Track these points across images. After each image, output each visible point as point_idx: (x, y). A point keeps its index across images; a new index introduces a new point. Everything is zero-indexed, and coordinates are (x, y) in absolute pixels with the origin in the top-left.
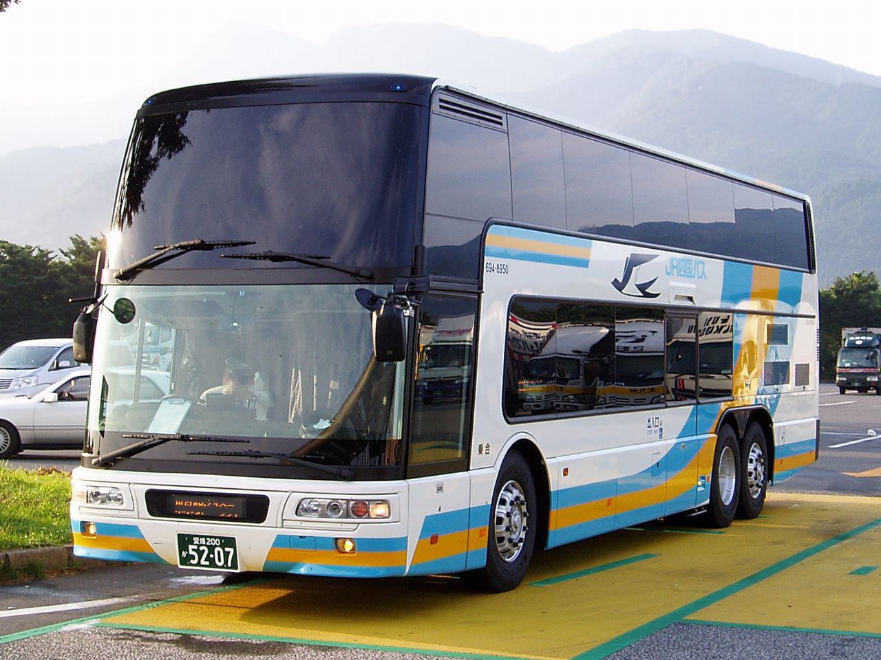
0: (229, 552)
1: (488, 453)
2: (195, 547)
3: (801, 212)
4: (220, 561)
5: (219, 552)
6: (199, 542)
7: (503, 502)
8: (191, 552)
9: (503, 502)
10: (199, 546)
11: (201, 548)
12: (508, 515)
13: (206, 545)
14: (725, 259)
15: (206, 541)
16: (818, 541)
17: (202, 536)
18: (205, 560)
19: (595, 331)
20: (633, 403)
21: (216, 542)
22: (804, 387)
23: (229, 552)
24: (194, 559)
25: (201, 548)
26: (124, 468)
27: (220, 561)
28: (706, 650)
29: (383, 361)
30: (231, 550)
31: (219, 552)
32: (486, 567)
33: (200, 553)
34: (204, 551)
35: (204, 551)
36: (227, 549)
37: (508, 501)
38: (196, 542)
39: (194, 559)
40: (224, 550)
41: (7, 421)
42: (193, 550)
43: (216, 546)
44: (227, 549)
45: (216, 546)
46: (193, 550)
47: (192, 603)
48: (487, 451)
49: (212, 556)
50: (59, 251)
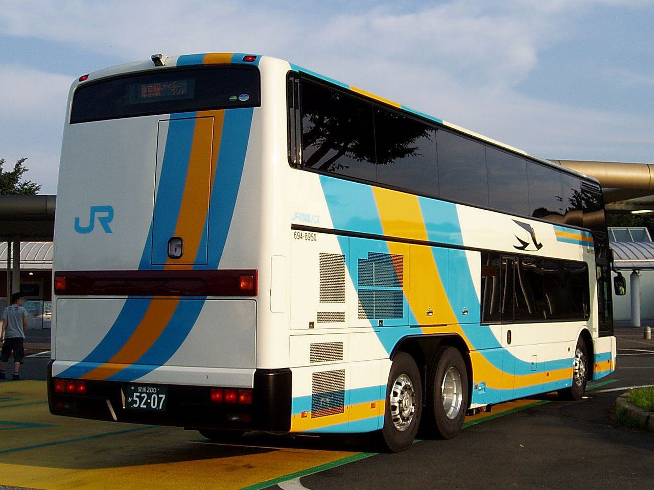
0: (162, 398)
2: (139, 394)
3: (171, 116)
4: (154, 405)
5: (154, 398)
6: (142, 390)
7: (395, 394)
8: (135, 398)
9: (395, 394)
10: (141, 393)
11: (142, 395)
12: (400, 402)
13: (146, 393)
14: (581, 230)
15: (147, 390)
20: (610, 364)
23: (162, 398)
24: (136, 404)
25: (142, 395)
27: (154, 405)
28: (509, 460)
29: (594, 247)
31: (154, 398)
33: (141, 399)
34: (144, 397)
35: (144, 397)
36: (160, 396)
37: (399, 392)
38: (140, 391)
39: (136, 404)
40: (158, 396)
42: (137, 396)
43: (153, 393)
44: (160, 396)
46: (137, 396)
47: (135, 430)
49: (149, 401)
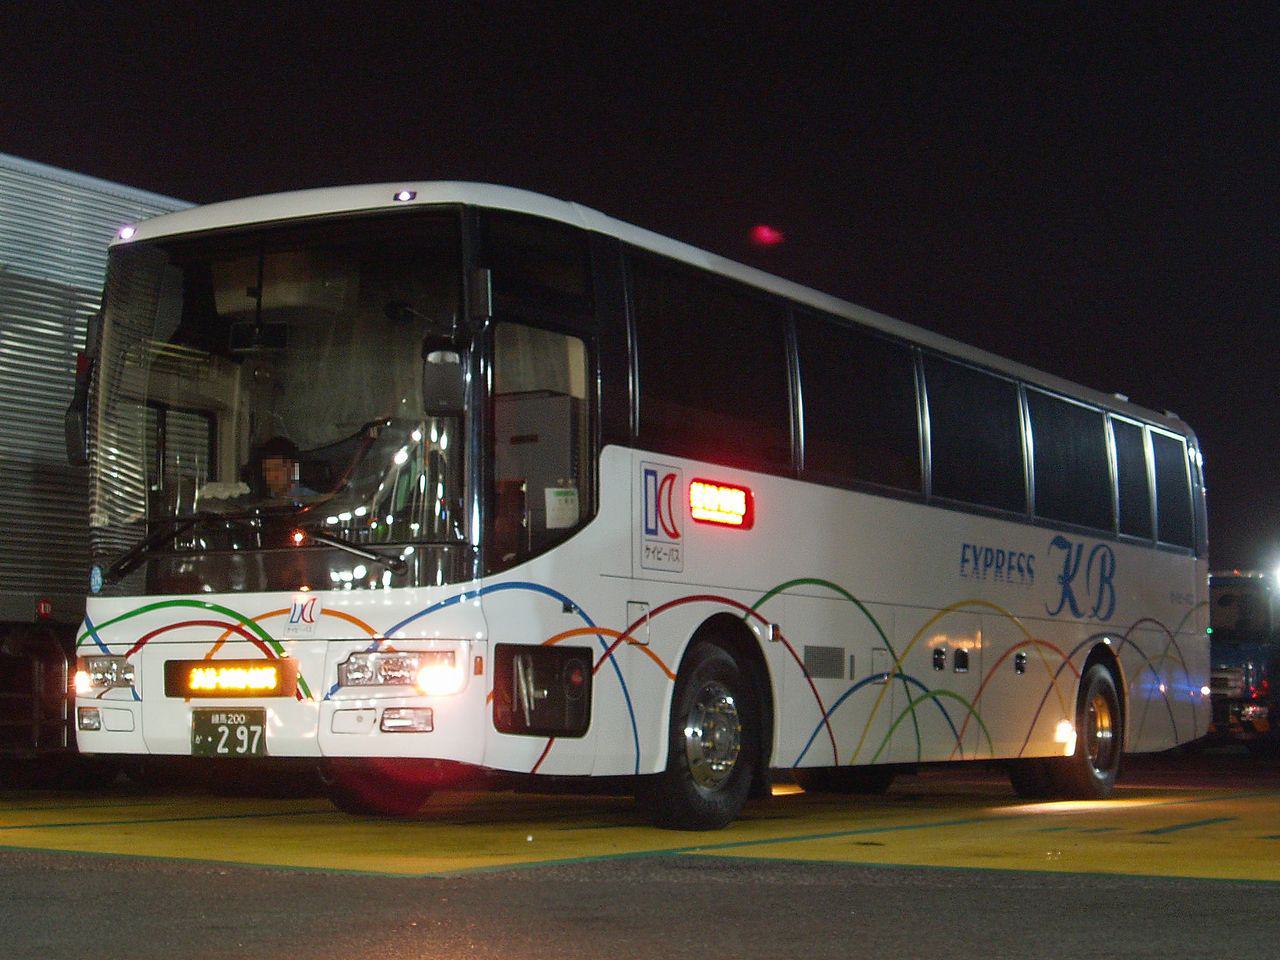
1: (938, 663)
15: (228, 718)
16: (407, 477)
17: (222, 712)
18: (255, 732)
19: (778, 751)
21: (240, 719)
22: (1204, 603)
26: (586, 703)
30: (258, 729)
32: (604, 445)
34: (223, 732)
35: (223, 732)
36: (253, 728)
41: (589, 719)
43: (239, 725)
44: (253, 728)
45: (239, 725)
48: (949, 661)
50: (882, 842)
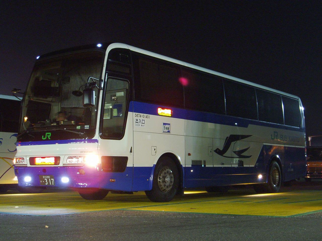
36: (52, 179)
44: (52, 179)
